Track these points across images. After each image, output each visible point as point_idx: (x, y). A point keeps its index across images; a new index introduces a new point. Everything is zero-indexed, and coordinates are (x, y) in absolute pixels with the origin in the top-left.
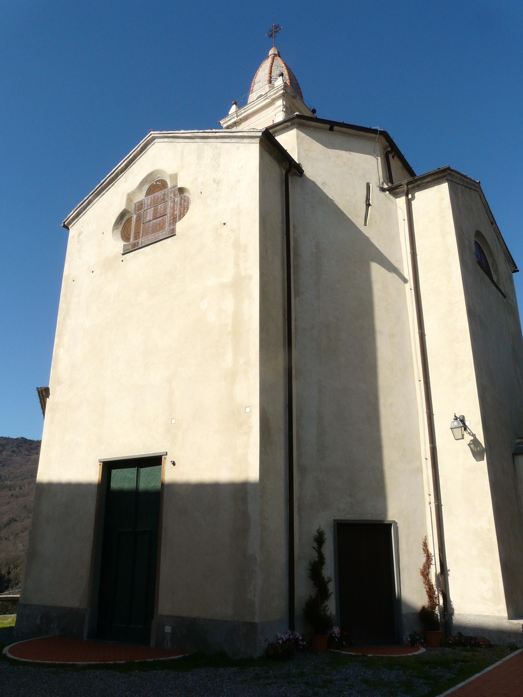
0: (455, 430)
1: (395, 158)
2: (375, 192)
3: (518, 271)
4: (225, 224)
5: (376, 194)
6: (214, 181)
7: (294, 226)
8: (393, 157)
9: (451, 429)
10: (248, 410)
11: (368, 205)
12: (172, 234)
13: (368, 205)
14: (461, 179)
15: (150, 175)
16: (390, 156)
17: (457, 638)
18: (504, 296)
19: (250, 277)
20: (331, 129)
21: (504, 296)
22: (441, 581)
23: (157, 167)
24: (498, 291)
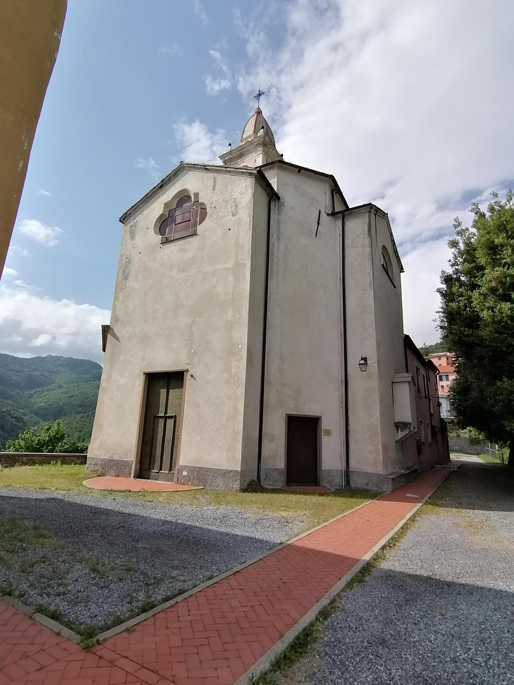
0: (361, 366)
1: (337, 194)
2: (324, 216)
3: (404, 272)
4: (229, 229)
5: (324, 218)
6: (224, 201)
7: (272, 234)
8: (336, 193)
9: (359, 364)
10: (240, 346)
11: (318, 224)
12: (195, 234)
13: (318, 224)
14: (382, 214)
15: (180, 193)
16: (334, 192)
17: (185, 473)
18: (395, 287)
19: (245, 265)
20: (299, 172)
21: (395, 287)
22: (12, 419)
23: (185, 187)
24: (392, 285)
